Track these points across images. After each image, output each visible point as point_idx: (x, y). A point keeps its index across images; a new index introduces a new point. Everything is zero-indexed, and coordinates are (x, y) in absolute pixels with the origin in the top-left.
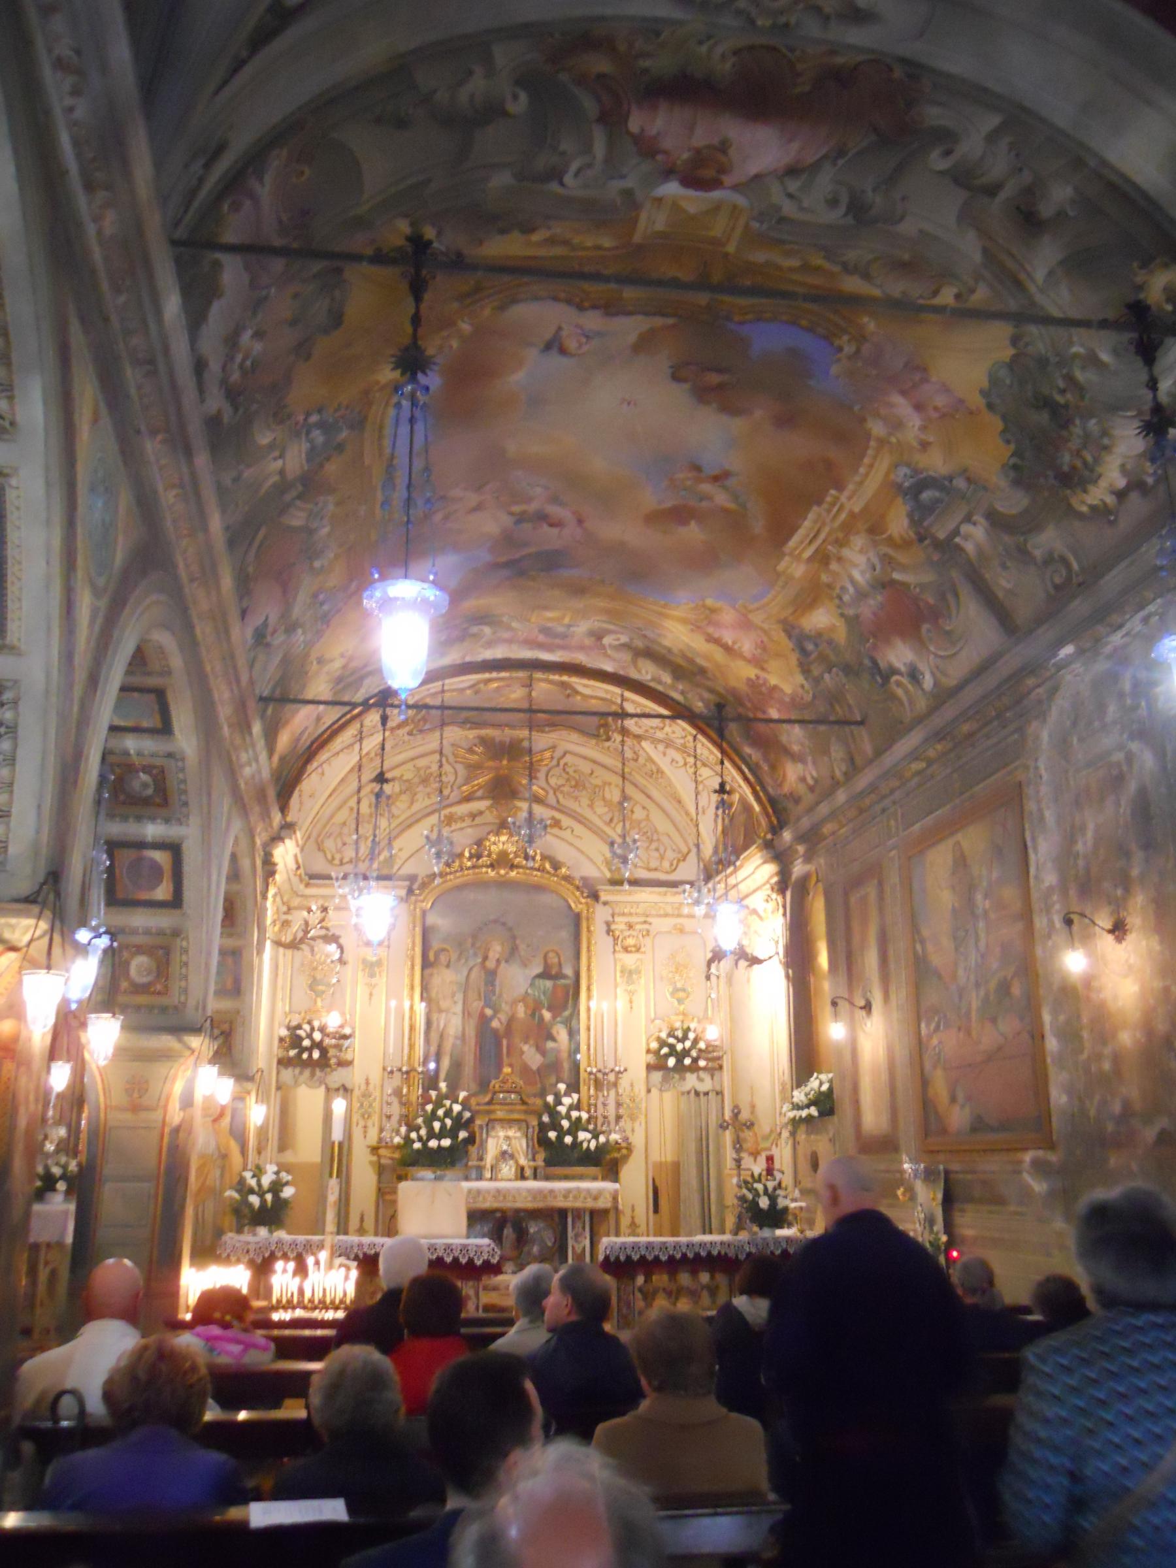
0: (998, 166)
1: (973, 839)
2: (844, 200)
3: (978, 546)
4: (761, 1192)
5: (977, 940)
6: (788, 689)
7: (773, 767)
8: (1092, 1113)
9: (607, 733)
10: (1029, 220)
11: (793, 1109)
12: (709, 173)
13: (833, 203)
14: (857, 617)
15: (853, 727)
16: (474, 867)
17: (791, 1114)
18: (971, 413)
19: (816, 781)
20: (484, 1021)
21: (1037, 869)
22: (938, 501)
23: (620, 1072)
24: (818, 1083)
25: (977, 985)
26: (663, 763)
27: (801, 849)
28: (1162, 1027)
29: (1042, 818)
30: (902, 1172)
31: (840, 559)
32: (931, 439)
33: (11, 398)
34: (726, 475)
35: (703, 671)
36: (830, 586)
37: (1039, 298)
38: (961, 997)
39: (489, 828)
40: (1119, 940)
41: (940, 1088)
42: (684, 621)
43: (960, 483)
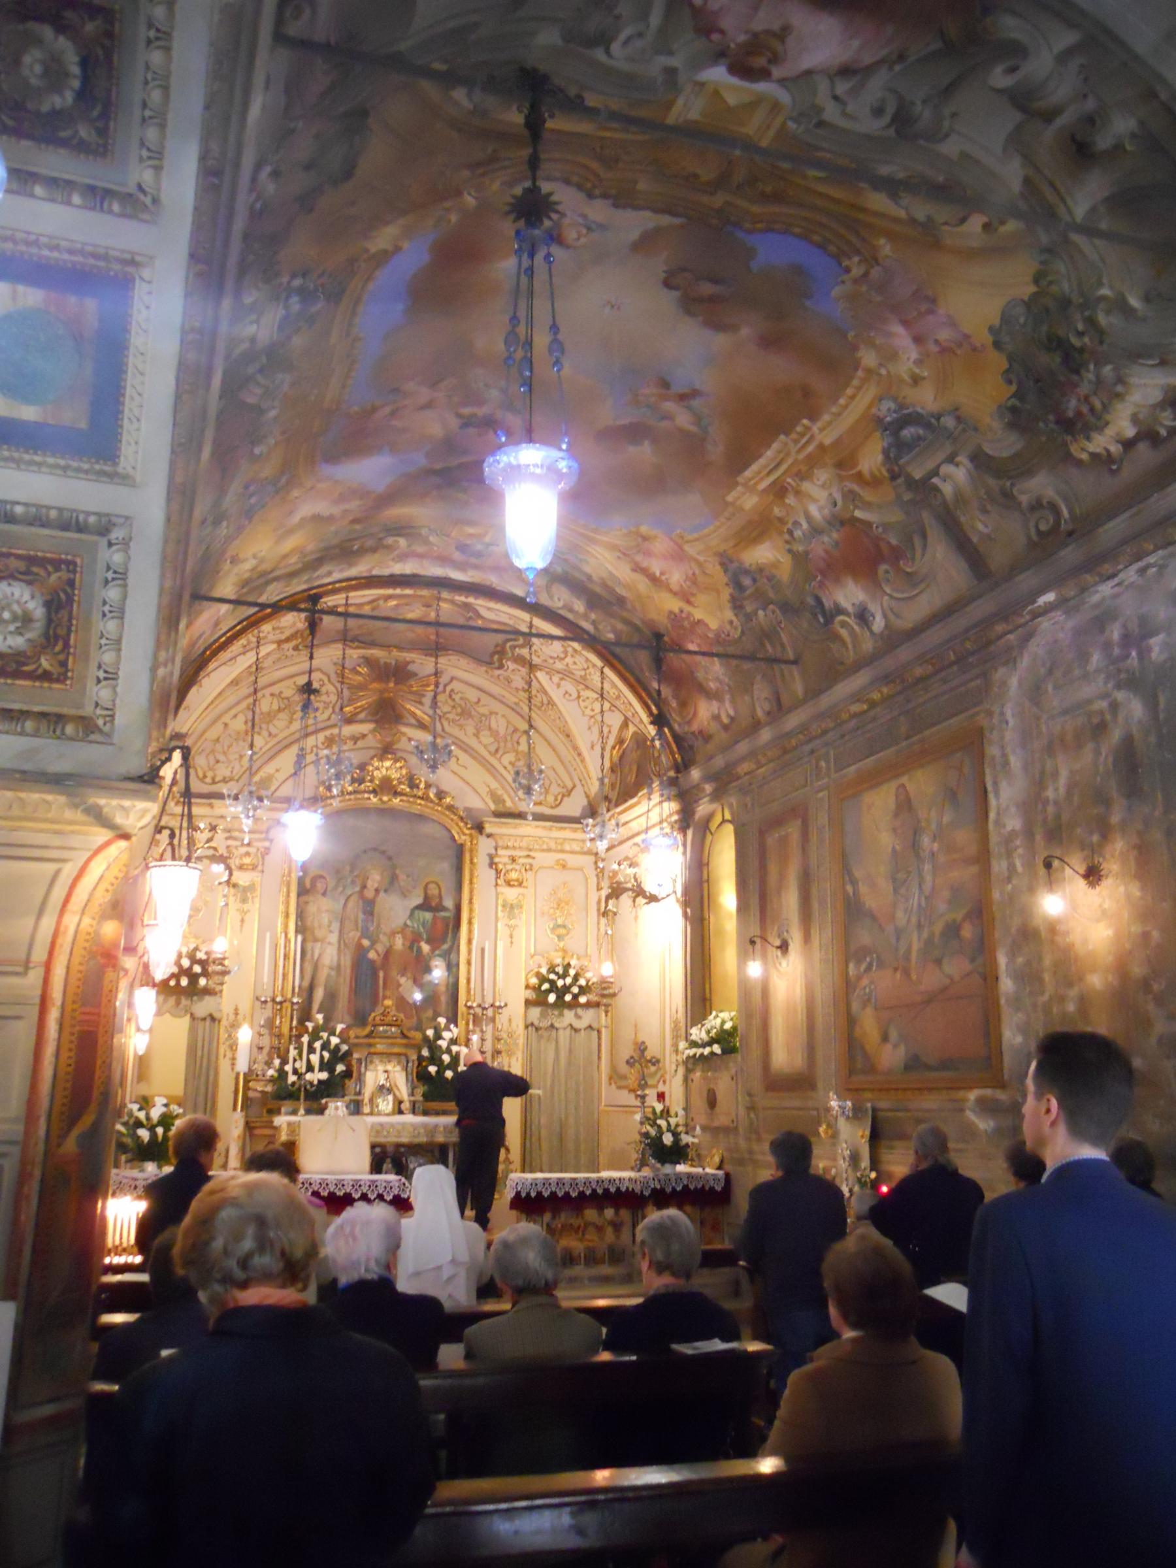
0: (1062, 90)
1: (922, 783)
2: (890, 110)
4: (664, 1129)
6: (714, 625)
7: (683, 704)
9: (500, 661)
10: (1080, 151)
11: (690, 1047)
12: (760, 62)
13: (878, 112)
14: (807, 553)
15: (783, 666)
16: (355, 792)
17: (691, 1052)
18: (974, 349)
19: (732, 719)
20: (360, 955)
21: (998, 814)
22: (919, 438)
23: (500, 1007)
25: (919, 926)
26: (556, 695)
27: (708, 788)
28: (1138, 970)
29: (1006, 764)
30: (828, 1110)
31: (798, 493)
33: (158, 169)
34: (695, 393)
35: (621, 601)
36: (781, 521)
38: (898, 939)
39: (372, 752)
41: (869, 1026)
42: (613, 548)
43: (949, 422)
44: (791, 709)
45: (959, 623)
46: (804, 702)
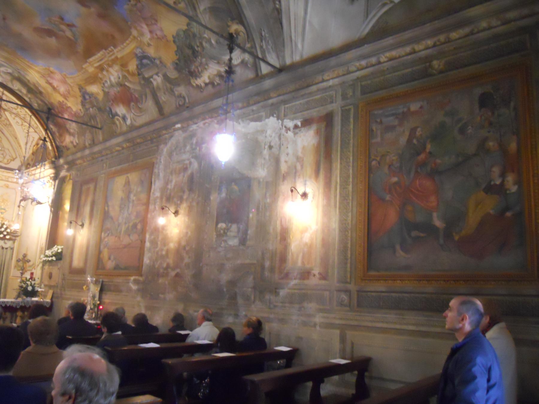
1: (134, 177)
3: (158, 83)
5: (129, 208)
7: (61, 135)
8: (157, 266)
14: (108, 92)
15: (97, 129)
17: (44, 259)
18: (167, 41)
19: (77, 144)
21: (154, 191)
22: (148, 64)
24: (57, 249)
25: (125, 223)
27: (66, 167)
28: (183, 243)
29: (159, 175)
31: (107, 71)
32: (152, 44)
35: (41, 93)
36: (101, 79)
37: (200, 15)
38: (119, 226)
40: (176, 216)
41: (105, 254)
42: (38, 72)
43: (158, 62)
44: (96, 145)
45: (151, 128)
46: (101, 143)
